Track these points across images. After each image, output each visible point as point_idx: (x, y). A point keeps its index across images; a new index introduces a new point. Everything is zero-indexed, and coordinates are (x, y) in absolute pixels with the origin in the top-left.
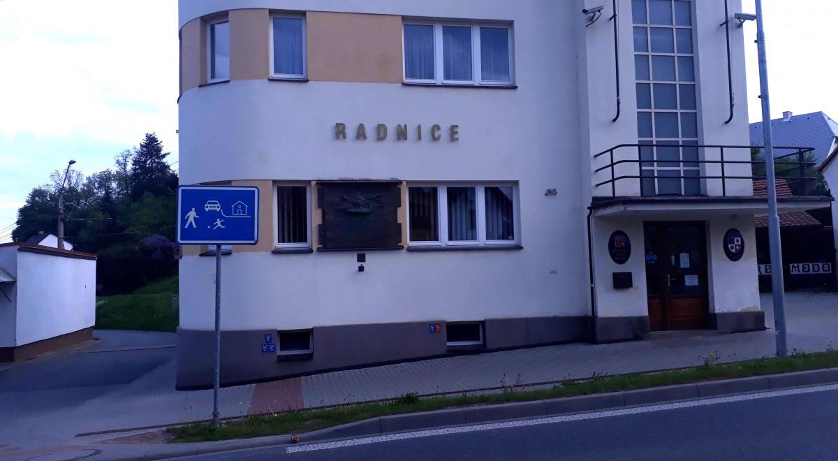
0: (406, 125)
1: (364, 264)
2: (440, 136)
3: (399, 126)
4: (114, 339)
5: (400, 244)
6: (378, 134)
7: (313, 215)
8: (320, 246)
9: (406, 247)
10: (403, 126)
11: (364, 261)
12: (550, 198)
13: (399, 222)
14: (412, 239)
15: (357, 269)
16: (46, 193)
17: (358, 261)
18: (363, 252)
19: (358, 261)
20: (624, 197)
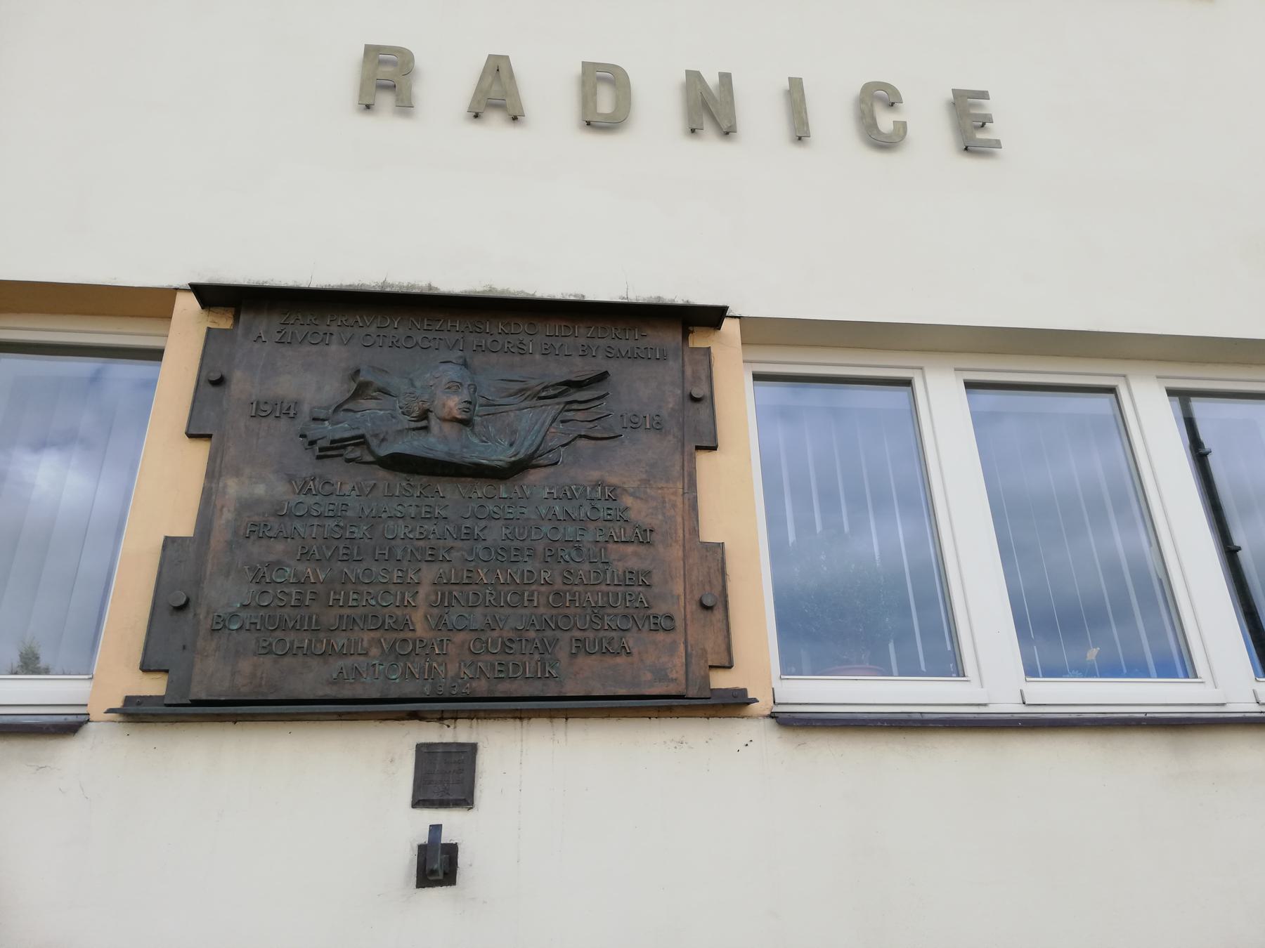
0: (726, 78)
1: (453, 823)
2: (902, 127)
3: (694, 78)
4: (440, 845)
5: (721, 681)
6: (587, 97)
7: (1124, 466)
8: (154, 686)
9: (763, 705)
10: (712, 80)
11: (465, 800)
12: (516, 113)
13: (710, 533)
14: (790, 666)
15: (407, 861)
16: (372, 385)
17: (420, 801)
18: (460, 733)
19: (420, 801)
20: (1224, 518)
